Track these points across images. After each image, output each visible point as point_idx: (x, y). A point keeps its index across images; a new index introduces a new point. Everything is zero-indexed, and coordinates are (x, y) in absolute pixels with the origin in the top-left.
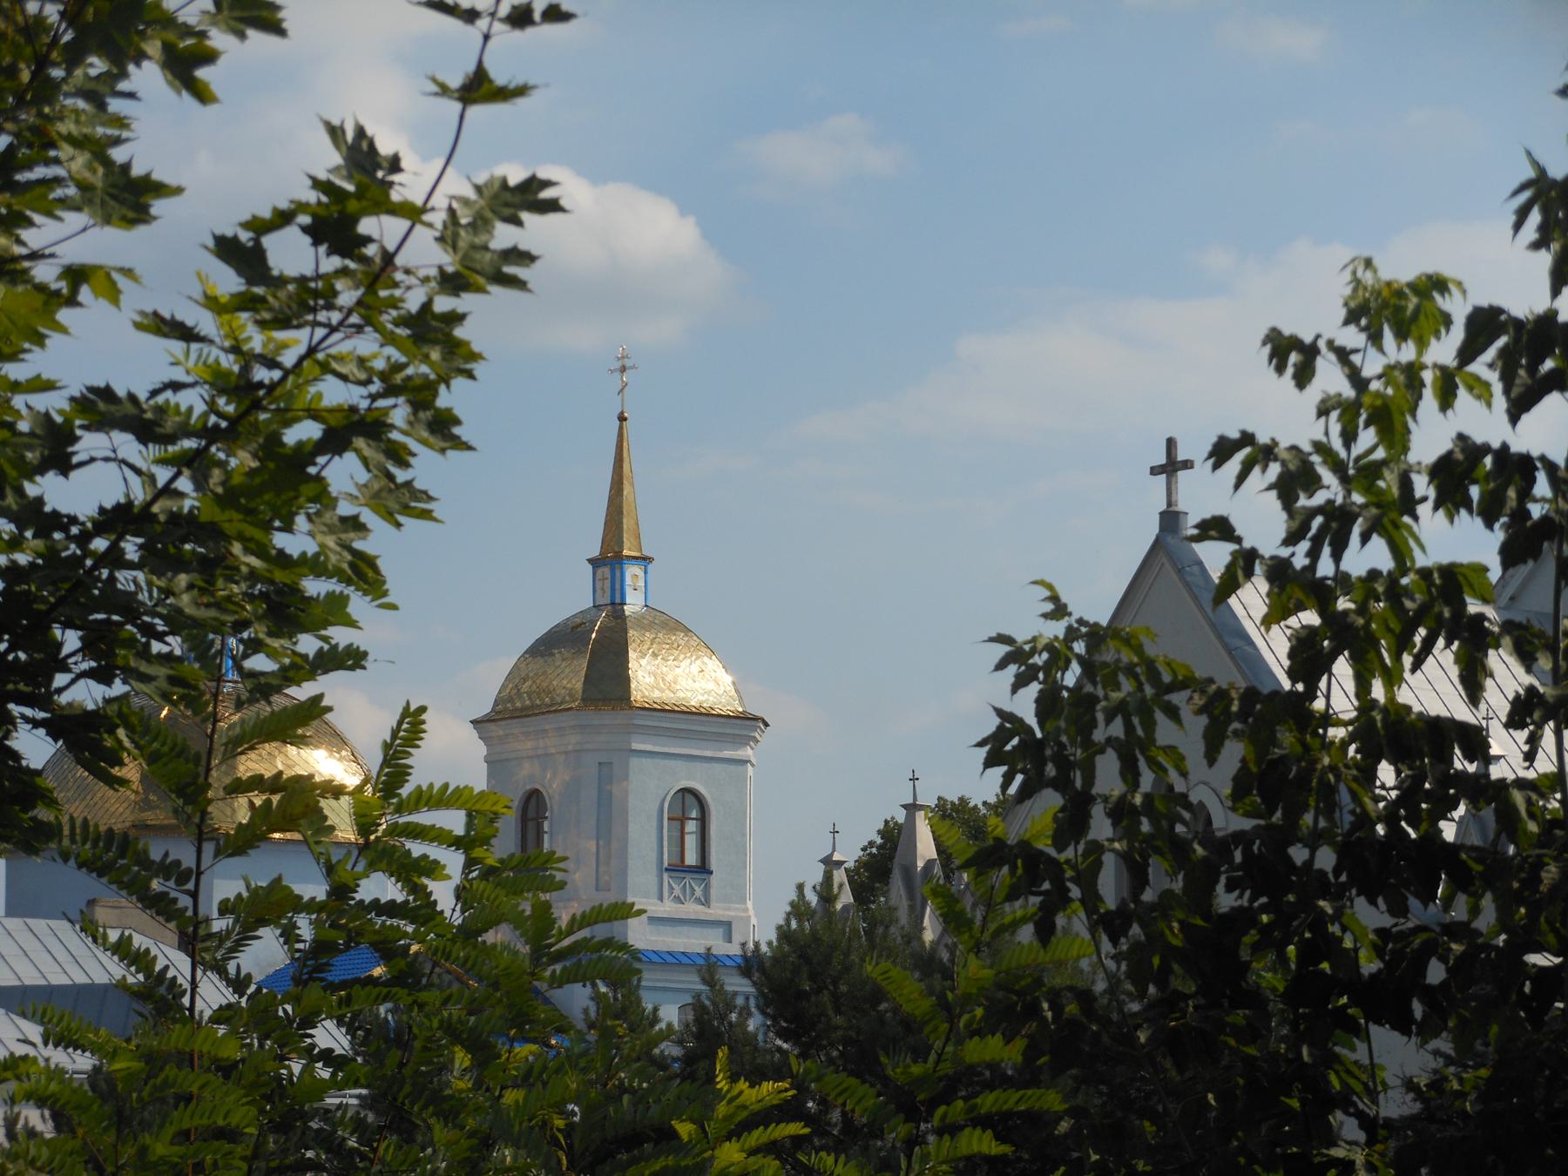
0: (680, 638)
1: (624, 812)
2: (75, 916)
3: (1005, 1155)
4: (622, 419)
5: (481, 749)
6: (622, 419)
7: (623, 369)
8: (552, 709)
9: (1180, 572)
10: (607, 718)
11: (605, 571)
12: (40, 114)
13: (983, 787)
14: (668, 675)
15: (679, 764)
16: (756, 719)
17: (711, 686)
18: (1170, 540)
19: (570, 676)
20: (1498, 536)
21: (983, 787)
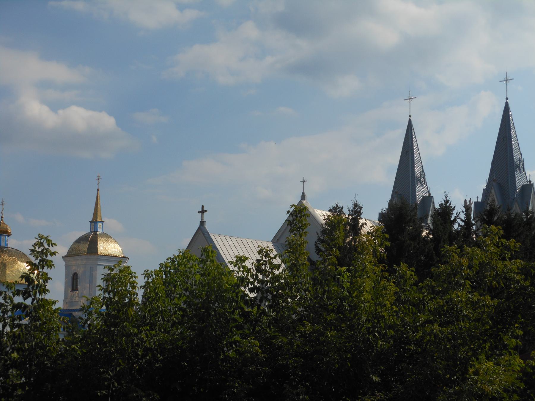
0: (110, 240)
1: (96, 278)
3: (516, 190)
4: (98, 190)
5: (64, 263)
6: (98, 190)
7: (99, 179)
8: (80, 255)
9: (203, 234)
10: (93, 257)
11: (93, 224)
14: (108, 247)
16: (126, 258)
17: (116, 250)
18: (202, 227)
19: (84, 247)
20: (21, 296)
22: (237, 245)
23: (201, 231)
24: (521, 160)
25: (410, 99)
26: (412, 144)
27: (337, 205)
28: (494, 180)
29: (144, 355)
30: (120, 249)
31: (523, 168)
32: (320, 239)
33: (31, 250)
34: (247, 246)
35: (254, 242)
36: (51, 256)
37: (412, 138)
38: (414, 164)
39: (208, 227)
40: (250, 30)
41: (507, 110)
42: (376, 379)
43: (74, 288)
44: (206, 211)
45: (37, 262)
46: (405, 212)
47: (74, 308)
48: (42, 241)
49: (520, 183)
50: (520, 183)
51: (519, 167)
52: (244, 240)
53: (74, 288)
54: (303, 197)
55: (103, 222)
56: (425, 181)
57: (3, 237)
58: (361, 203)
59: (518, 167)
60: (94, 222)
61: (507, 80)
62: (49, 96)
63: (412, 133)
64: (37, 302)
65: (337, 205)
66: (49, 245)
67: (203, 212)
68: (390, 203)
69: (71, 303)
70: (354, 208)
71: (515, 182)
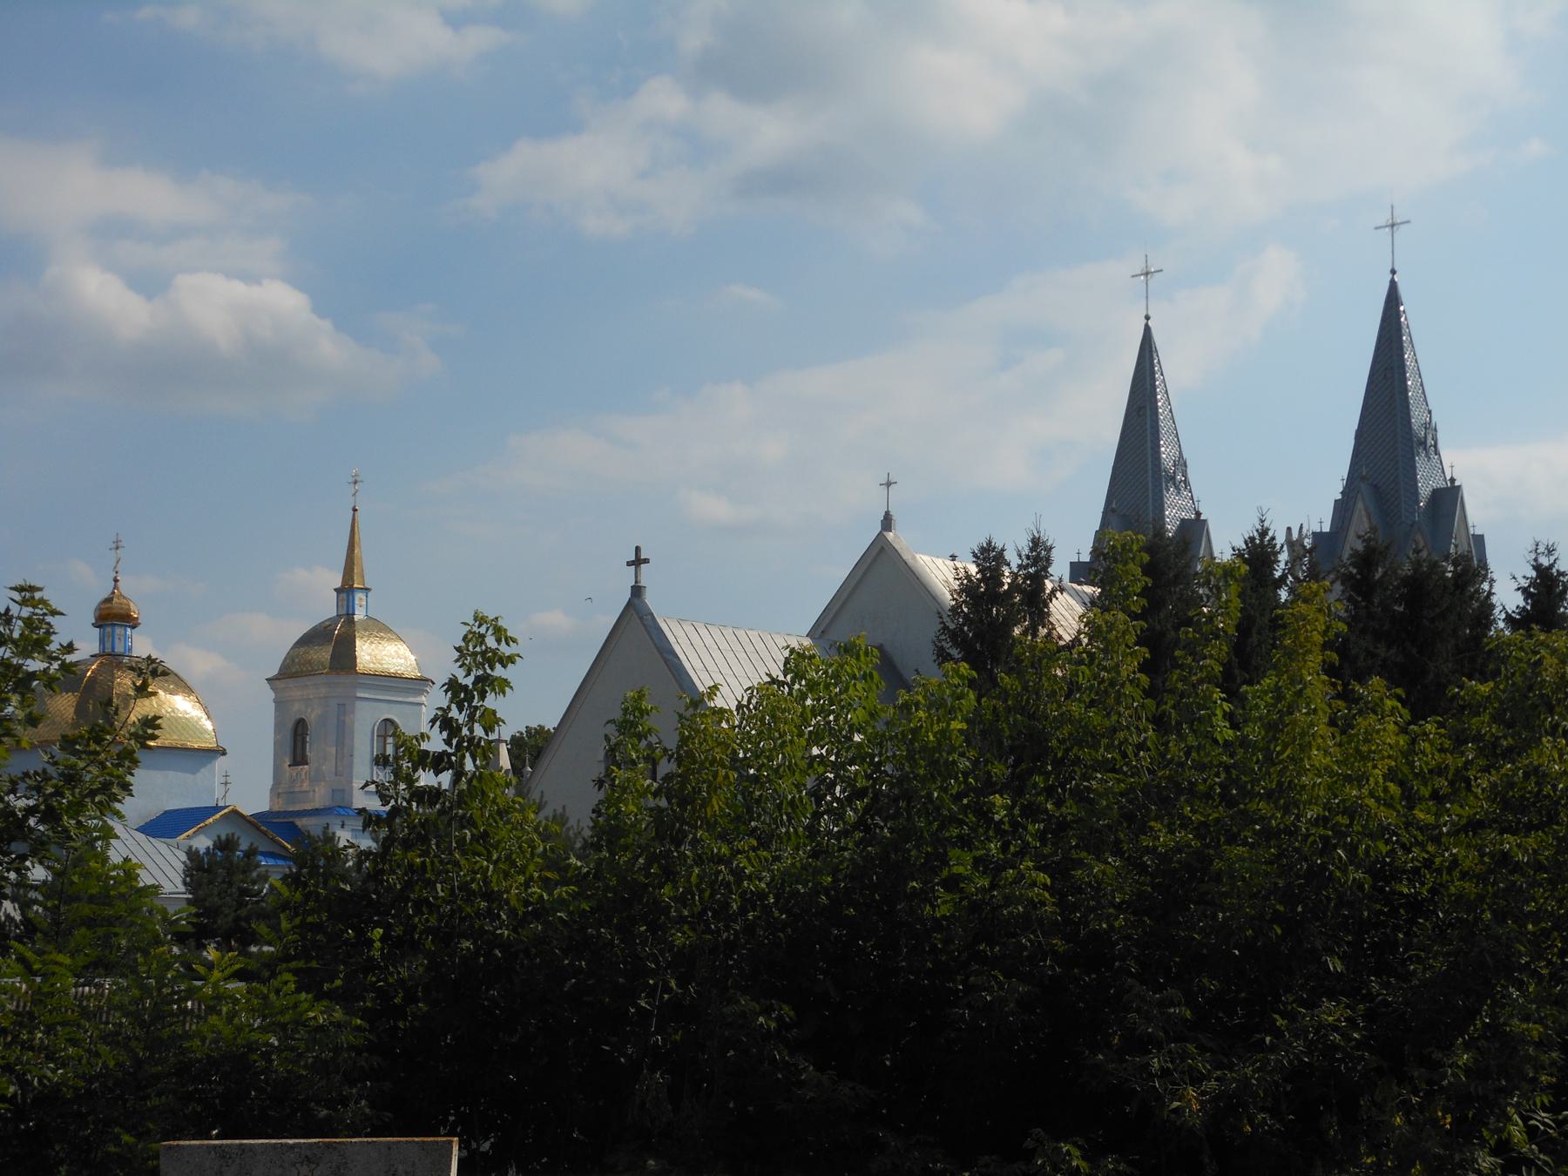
1: (353, 732)
2: (842, 634)
3: (1418, 502)
4: (355, 510)
5: (272, 695)
6: (355, 510)
9: (641, 619)
11: (344, 595)
12: (1179, 724)
13: (1225, 542)
14: (372, 654)
15: (384, 705)
18: (636, 601)
19: (324, 654)
21: (1225, 542)
22: (724, 645)
23: (635, 612)
24: (1429, 426)
25: (1147, 274)
26: (1154, 387)
27: (989, 543)
28: (1363, 478)
29: (743, 911)
30: (413, 658)
31: (1435, 446)
32: (945, 628)
33: (458, 649)
34: (749, 649)
35: (767, 638)
36: (504, 666)
37: (1153, 373)
38: (1158, 440)
39: (650, 600)
40: (664, 99)
41: (1393, 300)
42: (1335, 965)
43: (299, 759)
44: (646, 561)
45: (469, 681)
46: (1146, 554)
47: (297, 808)
48: (483, 630)
49: (1426, 484)
50: (1426, 484)
51: (1425, 443)
52: (741, 633)
53: (299, 759)
54: (887, 522)
55: (367, 590)
56: (1186, 482)
57: (118, 630)
58: (1050, 535)
59: (1423, 443)
60: (346, 590)
61: (1393, 225)
62: (177, 266)
63: (1152, 359)
64: (469, 782)
65: (989, 543)
66: (499, 641)
67: (638, 562)
68: (1099, 537)
69: (291, 795)
70: (1032, 550)
71: (1416, 481)
